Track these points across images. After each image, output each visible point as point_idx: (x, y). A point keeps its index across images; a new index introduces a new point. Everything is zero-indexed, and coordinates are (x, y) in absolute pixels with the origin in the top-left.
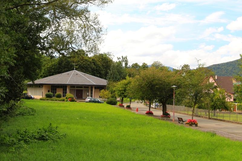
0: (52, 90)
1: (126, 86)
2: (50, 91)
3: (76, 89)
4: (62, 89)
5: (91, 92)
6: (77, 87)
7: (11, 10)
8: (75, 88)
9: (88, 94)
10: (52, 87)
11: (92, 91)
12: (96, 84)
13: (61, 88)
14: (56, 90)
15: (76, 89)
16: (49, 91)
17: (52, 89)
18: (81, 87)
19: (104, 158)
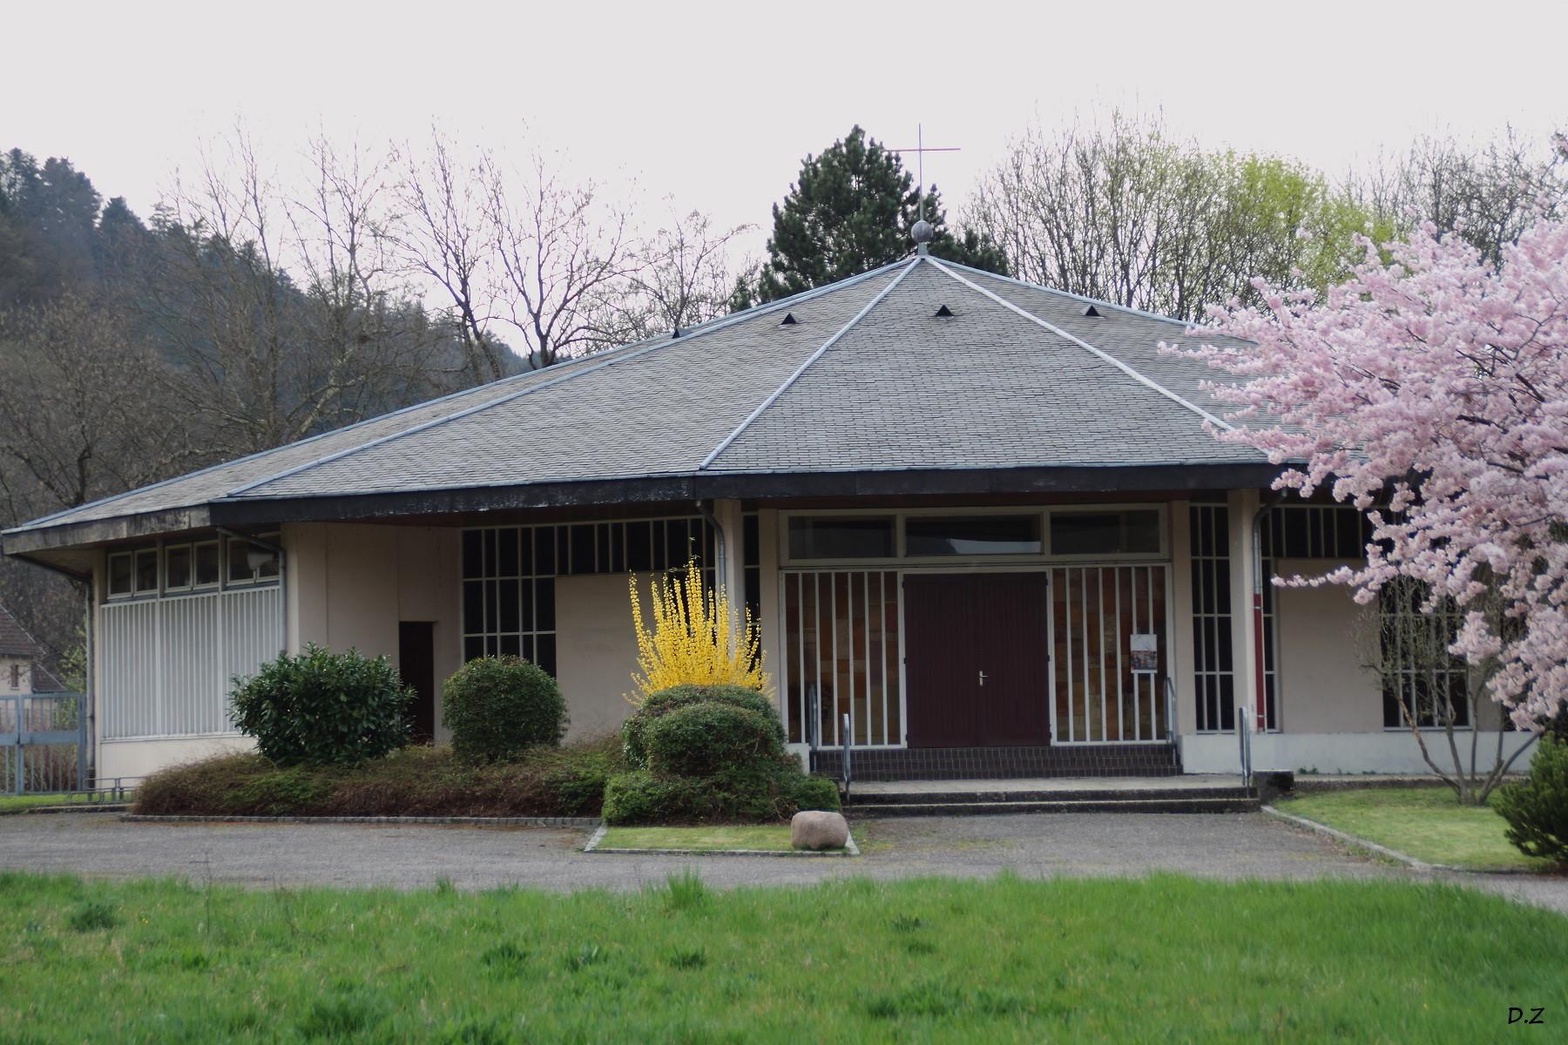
14: (548, 620)
15: (905, 565)
17: (472, 593)
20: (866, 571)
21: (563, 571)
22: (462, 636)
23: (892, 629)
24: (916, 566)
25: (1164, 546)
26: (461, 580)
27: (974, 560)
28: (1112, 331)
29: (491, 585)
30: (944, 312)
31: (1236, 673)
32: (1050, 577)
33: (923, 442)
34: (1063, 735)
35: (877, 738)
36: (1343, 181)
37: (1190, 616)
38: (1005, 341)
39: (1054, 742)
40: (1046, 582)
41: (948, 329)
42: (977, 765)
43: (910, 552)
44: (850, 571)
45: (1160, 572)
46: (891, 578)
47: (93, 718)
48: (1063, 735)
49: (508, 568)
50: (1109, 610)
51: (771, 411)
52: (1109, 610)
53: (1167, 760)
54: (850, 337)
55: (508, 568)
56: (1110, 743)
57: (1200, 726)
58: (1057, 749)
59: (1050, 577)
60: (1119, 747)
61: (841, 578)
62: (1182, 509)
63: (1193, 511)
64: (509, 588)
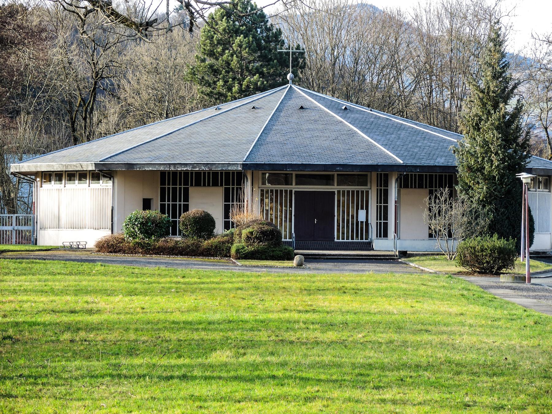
0: (163, 199)
1: (271, 329)
2: (156, 203)
3: (295, 188)
4: (219, 192)
5: (379, 209)
6: (302, 179)
7: (434, 102)
8: (288, 188)
9: (362, 216)
10: (163, 183)
11: (383, 197)
12: (411, 162)
13: (215, 184)
14: (186, 199)
15: (295, 188)
16: (147, 204)
17: (163, 191)
18: (327, 180)
19: (393, 343)
20: (284, 189)
21: (192, 185)
22: (159, 203)
23: (291, 206)
24: (298, 188)
25: (369, 184)
26: (160, 186)
27: (398, 221)
28: (353, 116)
29: (180, 189)
30: (302, 108)
31: (389, 221)
32: (336, 193)
33: (304, 154)
34: (338, 238)
35: (348, 239)
36: (413, 14)
37: (376, 204)
38: (322, 119)
39: (336, 240)
40: (335, 194)
41: (304, 113)
42: (357, 246)
43: (296, 184)
44: (279, 189)
45: (367, 192)
46: (291, 191)
47: (37, 222)
48: (338, 238)
49: (175, 183)
50: (353, 203)
51: (258, 142)
52: (353, 203)
53: (368, 246)
54: (275, 116)
55: (175, 183)
56: (352, 241)
57: (377, 237)
58: (283, 242)
59: (336, 193)
60: (287, 242)
61: (281, 191)
62: (374, 174)
63: (378, 174)
64: (174, 190)
